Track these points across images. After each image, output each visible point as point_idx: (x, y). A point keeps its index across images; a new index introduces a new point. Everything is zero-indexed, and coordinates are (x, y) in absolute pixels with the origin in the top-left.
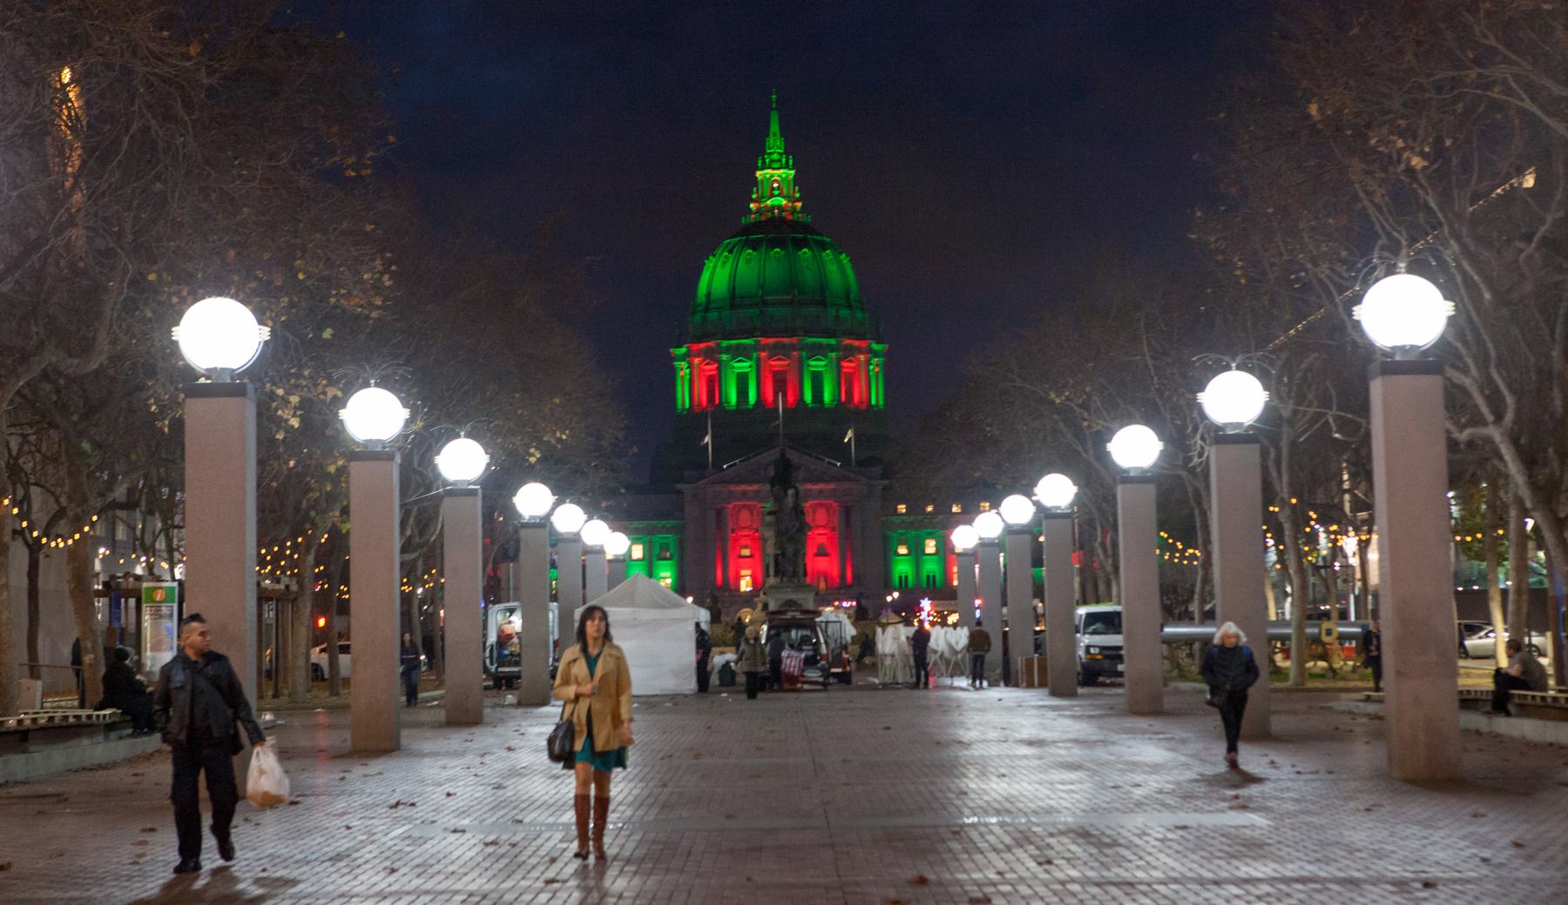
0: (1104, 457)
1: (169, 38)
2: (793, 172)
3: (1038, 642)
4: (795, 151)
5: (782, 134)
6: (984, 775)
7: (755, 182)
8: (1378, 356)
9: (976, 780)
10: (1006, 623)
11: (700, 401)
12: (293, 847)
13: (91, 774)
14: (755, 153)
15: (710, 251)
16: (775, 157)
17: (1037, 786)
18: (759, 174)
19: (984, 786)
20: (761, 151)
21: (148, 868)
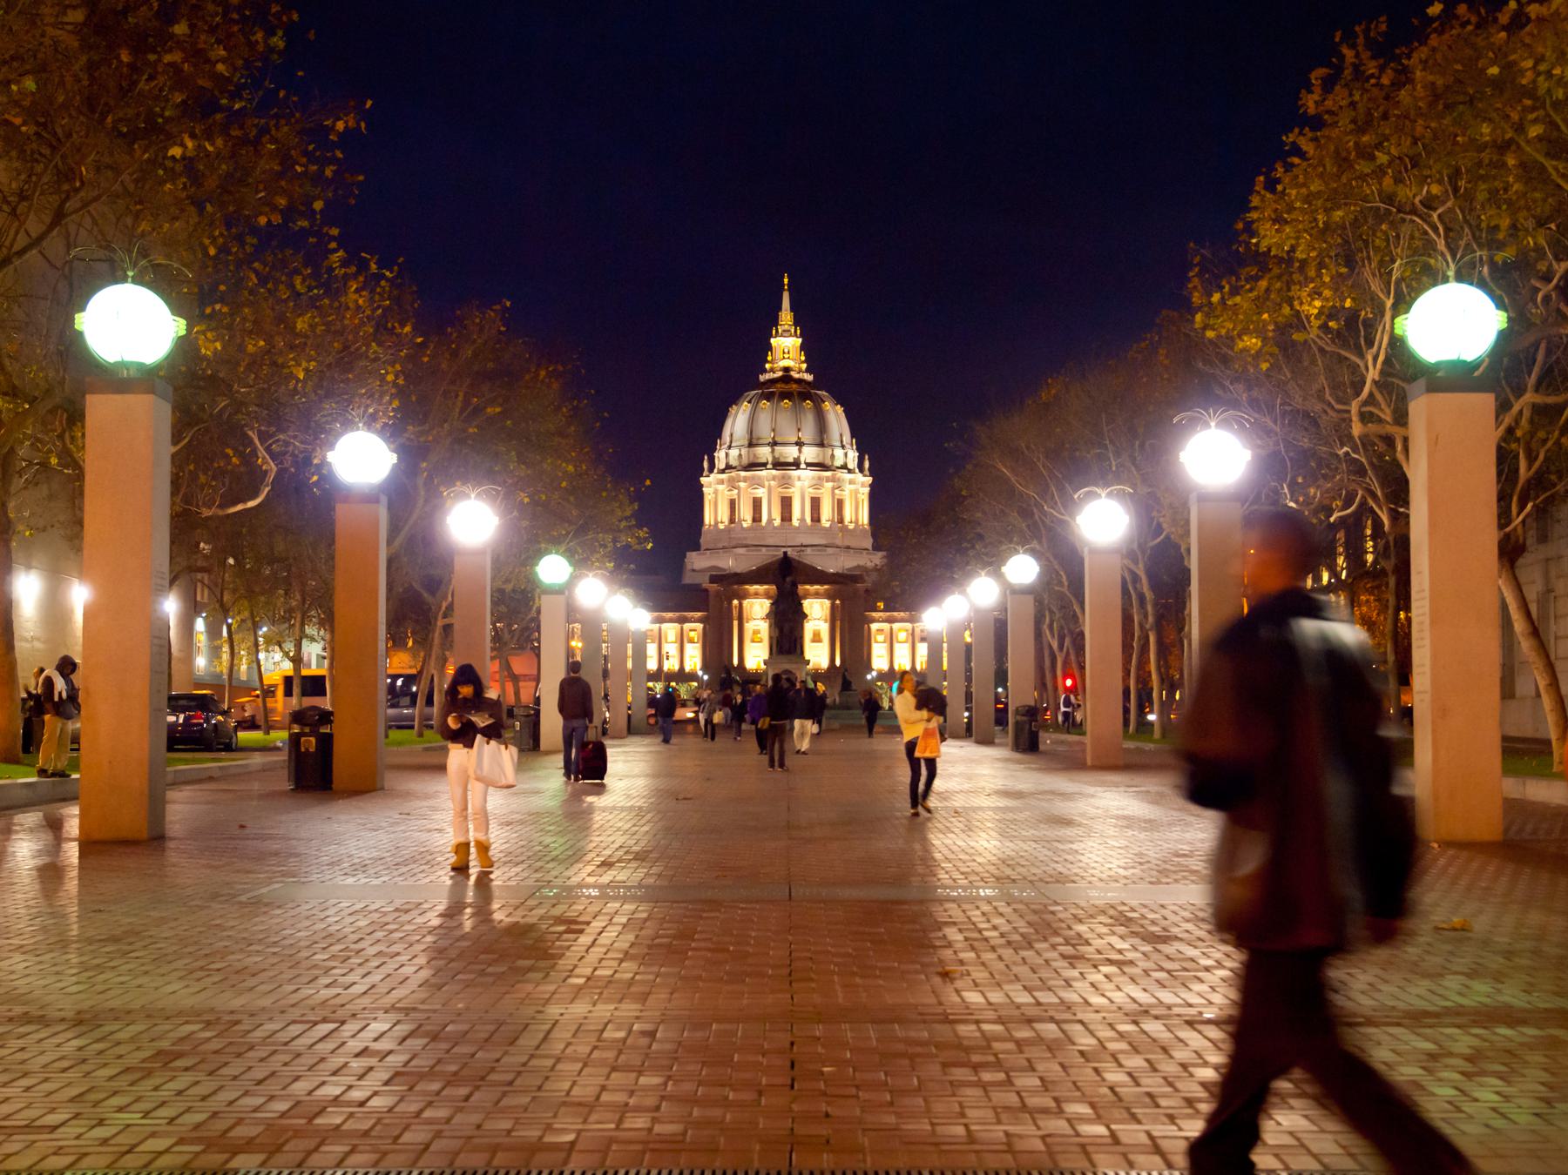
0: (539, 554)
1: (1232, 339)
2: (800, 340)
3: (1406, 721)
4: (802, 321)
5: (792, 309)
6: (970, 830)
7: (770, 347)
8: (401, 440)
9: (962, 835)
10: (629, 708)
11: (770, 520)
12: (396, 873)
13: (1041, 788)
14: (771, 322)
15: (735, 399)
16: (786, 327)
17: (1035, 845)
18: (773, 341)
19: (972, 844)
20: (775, 322)
21: (525, 874)
